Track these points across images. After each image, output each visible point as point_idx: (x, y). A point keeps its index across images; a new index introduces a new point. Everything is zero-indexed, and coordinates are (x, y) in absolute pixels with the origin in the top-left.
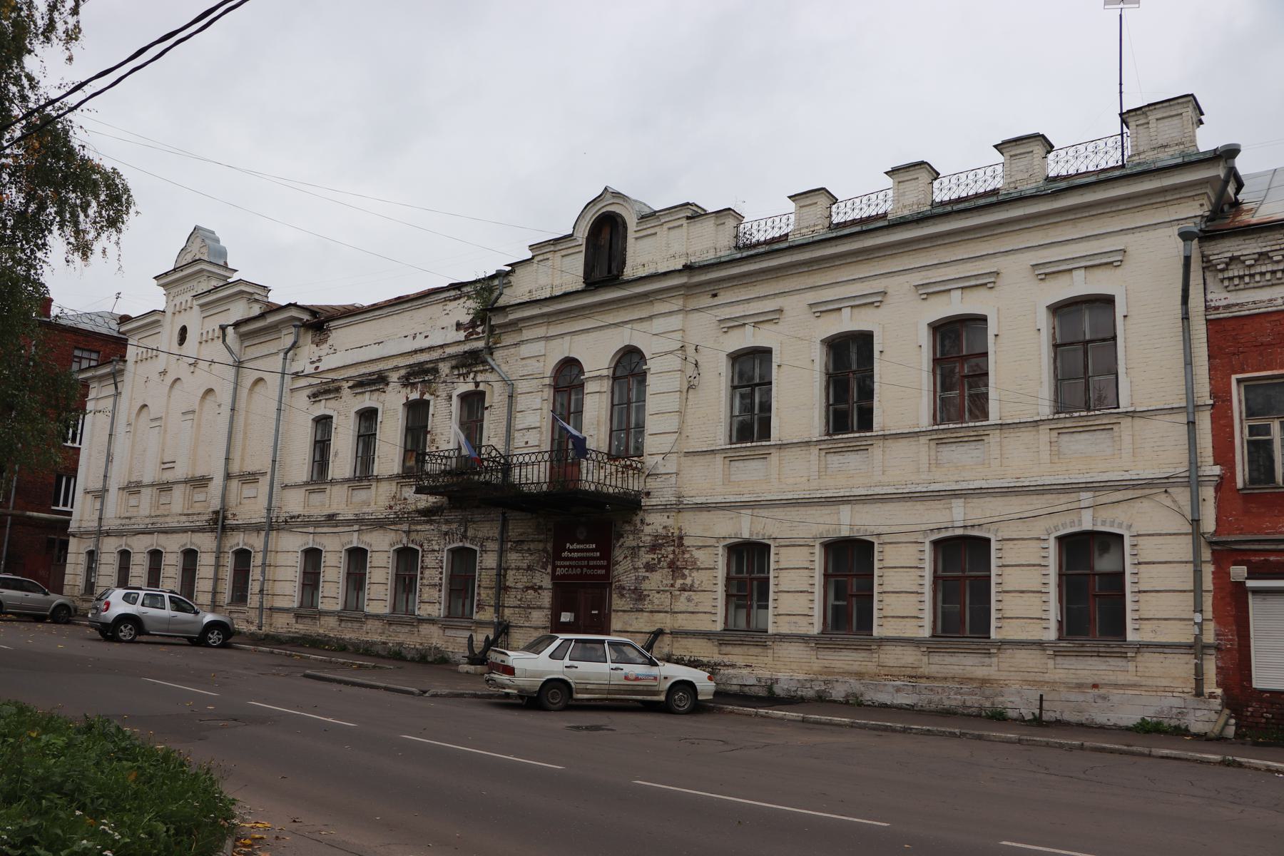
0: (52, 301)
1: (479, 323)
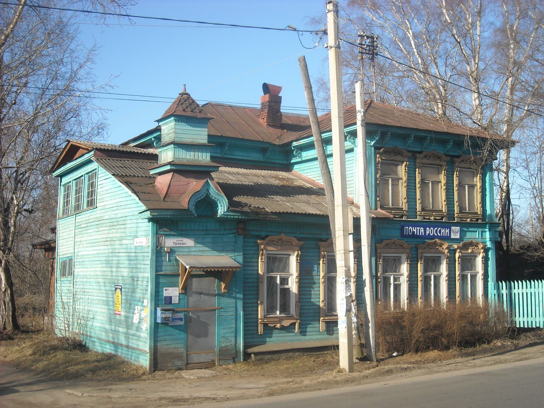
0: (279, 89)
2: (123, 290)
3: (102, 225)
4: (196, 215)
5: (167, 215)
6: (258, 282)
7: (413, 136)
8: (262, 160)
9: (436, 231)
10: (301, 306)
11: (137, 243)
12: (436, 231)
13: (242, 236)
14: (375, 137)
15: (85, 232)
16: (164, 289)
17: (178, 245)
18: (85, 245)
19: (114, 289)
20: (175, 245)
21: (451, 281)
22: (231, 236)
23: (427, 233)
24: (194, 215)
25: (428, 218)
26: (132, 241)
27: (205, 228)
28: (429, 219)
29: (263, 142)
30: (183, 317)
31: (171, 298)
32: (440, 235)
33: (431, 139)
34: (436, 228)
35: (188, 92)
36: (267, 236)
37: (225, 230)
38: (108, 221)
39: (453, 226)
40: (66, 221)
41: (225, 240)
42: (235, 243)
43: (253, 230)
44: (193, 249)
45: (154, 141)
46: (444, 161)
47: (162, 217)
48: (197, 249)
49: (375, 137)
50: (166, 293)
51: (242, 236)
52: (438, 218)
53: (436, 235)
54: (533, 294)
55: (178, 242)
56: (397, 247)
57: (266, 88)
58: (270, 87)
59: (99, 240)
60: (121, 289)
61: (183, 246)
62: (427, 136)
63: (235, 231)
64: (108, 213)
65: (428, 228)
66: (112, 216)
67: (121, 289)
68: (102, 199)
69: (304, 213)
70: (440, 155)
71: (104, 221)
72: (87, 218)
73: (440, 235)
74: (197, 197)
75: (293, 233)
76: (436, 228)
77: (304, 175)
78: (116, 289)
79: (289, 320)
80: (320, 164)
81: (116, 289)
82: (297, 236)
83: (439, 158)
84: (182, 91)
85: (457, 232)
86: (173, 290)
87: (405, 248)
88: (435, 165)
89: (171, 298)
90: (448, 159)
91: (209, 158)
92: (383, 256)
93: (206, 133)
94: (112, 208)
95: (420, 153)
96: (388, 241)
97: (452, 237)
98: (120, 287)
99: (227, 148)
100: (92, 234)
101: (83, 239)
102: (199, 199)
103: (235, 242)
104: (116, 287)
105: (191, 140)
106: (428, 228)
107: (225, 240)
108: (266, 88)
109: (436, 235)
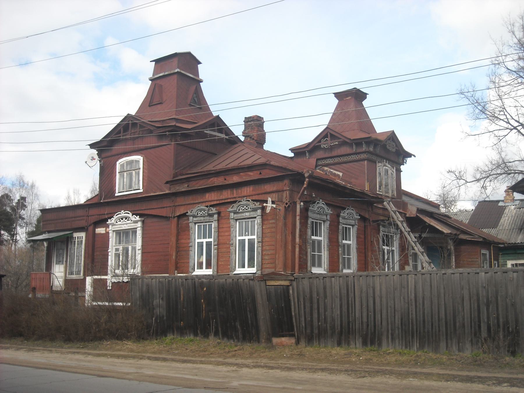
0: (245, 118)
39: (509, 260)
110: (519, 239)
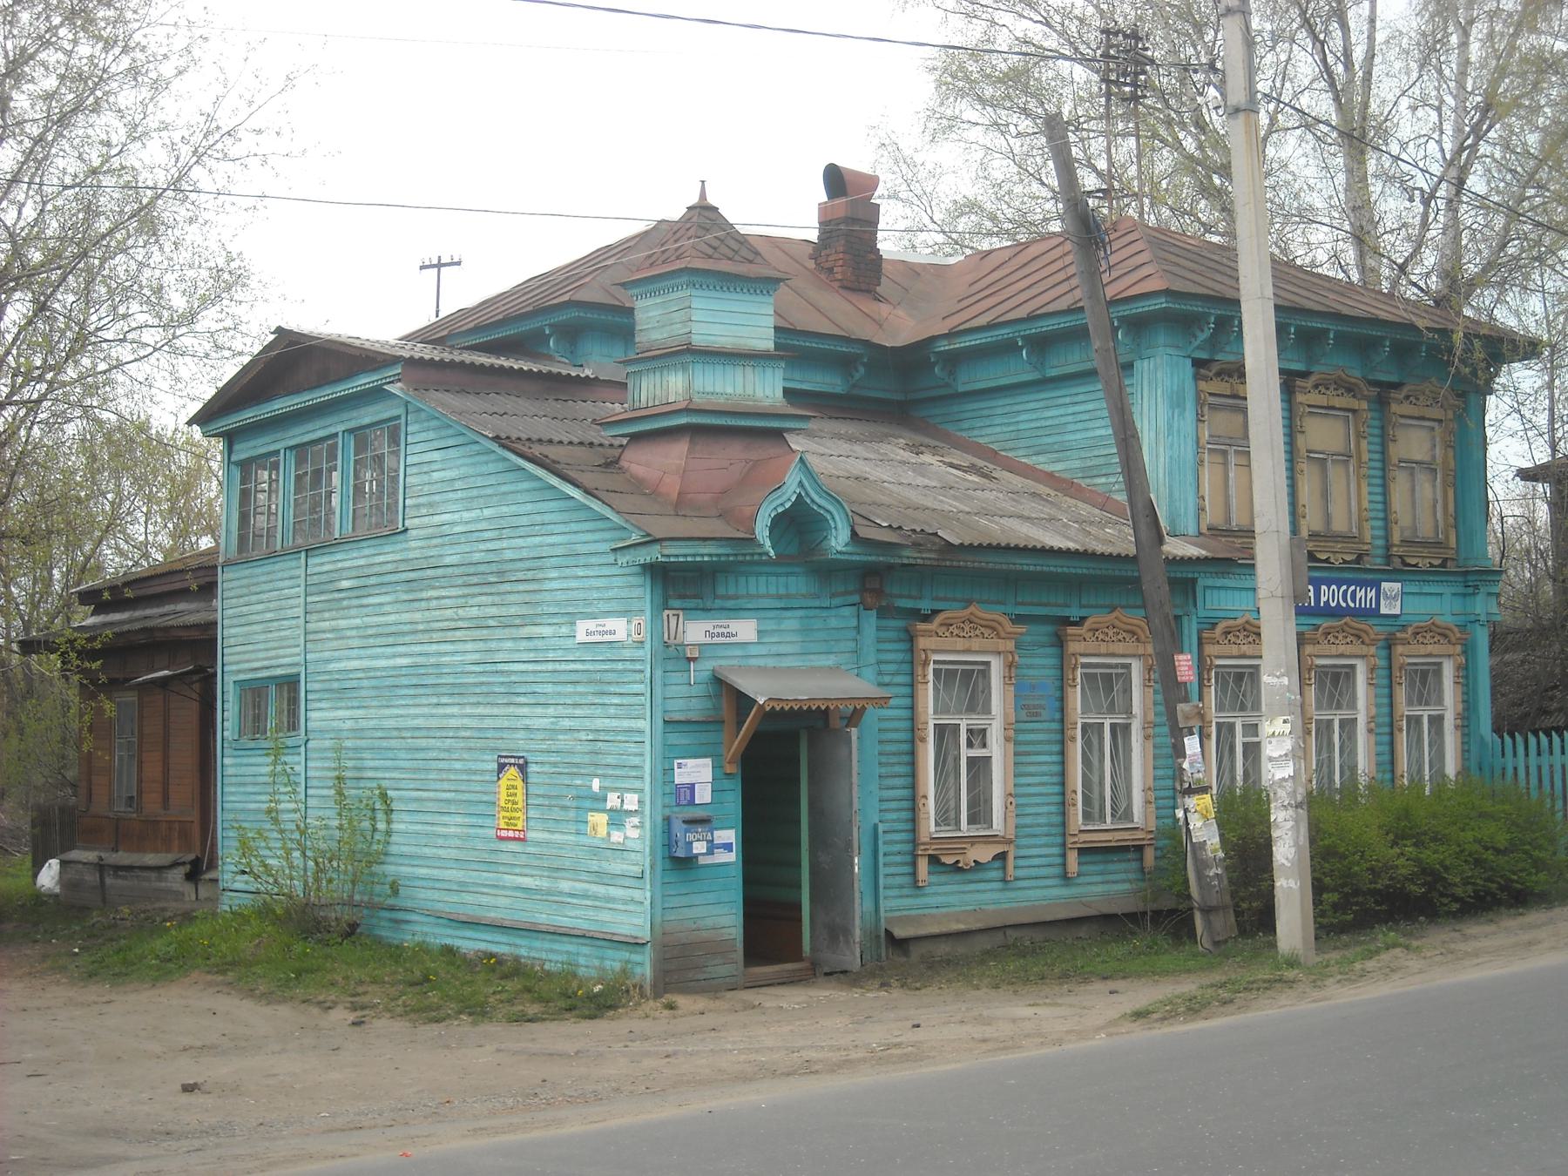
0: (704, 215)
1: (1164, 184)
2: (532, 768)
3: (433, 583)
4: (772, 553)
5: (702, 555)
6: (913, 742)
7: (1212, 319)
8: (839, 390)
9: (1345, 592)
10: (1017, 806)
11: (588, 634)
12: (1345, 592)
13: (874, 612)
14: (1198, 333)
15: (355, 602)
16: (676, 761)
17: (716, 640)
18: (356, 643)
19: (495, 766)
20: (708, 640)
21: (636, 755)
22: (847, 611)
23: (1323, 599)
24: (767, 554)
25: (1324, 557)
26: (564, 630)
27: (782, 591)
28: (1327, 561)
29: (847, 340)
30: (733, 840)
31: (692, 787)
32: (1352, 605)
33: (1339, 337)
34: (1344, 587)
35: (712, 200)
36: (935, 612)
37: (833, 596)
38: (457, 571)
40: (259, 570)
41: (833, 623)
42: (859, 632)
43: (901, 596)
44: (754, 650)
45: (549, 336)
46: (1365, 398)
47: (689, 559)
48: (763, 650)
49: (1198, 333)
50: (680, 774)
51: (874, 612)
52: (1348, 558)
53: (1344, 605)
54: (1545, 771)
55: (716, 631)
56: (1120, 637)
57: (836, 179)
58: (846, 178)
59: (421, 627)
60: (523, 768)
61: (728, 640)
62: (1328, 330)
63: (856, 598)
64: (458, 549)
65: (1324, 587)
66: (477, 557)
67: (523, 768)
68: (431, 505)
69: (1039, 546)
70: (1353, 380)
71: (440, 572)
72: (362, 562)
73: (1352, 605)
74: (774, 505)
75: (999, 603)
76: (1344, 587)
77: (959, 434)
78: (501, 767)
79: (989, 846)
80: (1111, 417)
81: (501, 767)
82: (1009, 609)
83: (1349, 390)
84: (694, 199)
85: (1395, 598)
86: (698, 766)
87: (1453, 640)
88: (1340, 409)
89: (692, 787)
90: (1374, 391)
91: (779, 393)
92: (935, 662)
93: (770, 322)
94: (476, 534)
95: (1305, 375)
96: (1231, 622)
97: (1384, 610)
98: (521, 761)
99: (862, 370)
100: (388, 608)
101: (343, 623)
102: (780, 510)
103: (858, 629)
104: (502, 760)
105: (730, 340)
106: (1324, 587)
107: (833, 623)
108: (836, 179)
109: (1344, 605)
110: (1366, 5)
